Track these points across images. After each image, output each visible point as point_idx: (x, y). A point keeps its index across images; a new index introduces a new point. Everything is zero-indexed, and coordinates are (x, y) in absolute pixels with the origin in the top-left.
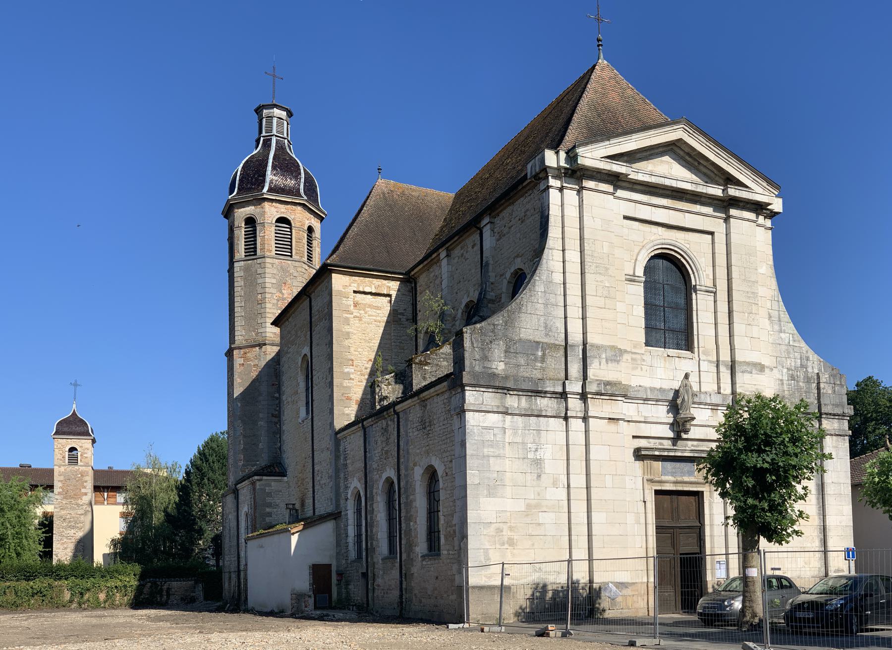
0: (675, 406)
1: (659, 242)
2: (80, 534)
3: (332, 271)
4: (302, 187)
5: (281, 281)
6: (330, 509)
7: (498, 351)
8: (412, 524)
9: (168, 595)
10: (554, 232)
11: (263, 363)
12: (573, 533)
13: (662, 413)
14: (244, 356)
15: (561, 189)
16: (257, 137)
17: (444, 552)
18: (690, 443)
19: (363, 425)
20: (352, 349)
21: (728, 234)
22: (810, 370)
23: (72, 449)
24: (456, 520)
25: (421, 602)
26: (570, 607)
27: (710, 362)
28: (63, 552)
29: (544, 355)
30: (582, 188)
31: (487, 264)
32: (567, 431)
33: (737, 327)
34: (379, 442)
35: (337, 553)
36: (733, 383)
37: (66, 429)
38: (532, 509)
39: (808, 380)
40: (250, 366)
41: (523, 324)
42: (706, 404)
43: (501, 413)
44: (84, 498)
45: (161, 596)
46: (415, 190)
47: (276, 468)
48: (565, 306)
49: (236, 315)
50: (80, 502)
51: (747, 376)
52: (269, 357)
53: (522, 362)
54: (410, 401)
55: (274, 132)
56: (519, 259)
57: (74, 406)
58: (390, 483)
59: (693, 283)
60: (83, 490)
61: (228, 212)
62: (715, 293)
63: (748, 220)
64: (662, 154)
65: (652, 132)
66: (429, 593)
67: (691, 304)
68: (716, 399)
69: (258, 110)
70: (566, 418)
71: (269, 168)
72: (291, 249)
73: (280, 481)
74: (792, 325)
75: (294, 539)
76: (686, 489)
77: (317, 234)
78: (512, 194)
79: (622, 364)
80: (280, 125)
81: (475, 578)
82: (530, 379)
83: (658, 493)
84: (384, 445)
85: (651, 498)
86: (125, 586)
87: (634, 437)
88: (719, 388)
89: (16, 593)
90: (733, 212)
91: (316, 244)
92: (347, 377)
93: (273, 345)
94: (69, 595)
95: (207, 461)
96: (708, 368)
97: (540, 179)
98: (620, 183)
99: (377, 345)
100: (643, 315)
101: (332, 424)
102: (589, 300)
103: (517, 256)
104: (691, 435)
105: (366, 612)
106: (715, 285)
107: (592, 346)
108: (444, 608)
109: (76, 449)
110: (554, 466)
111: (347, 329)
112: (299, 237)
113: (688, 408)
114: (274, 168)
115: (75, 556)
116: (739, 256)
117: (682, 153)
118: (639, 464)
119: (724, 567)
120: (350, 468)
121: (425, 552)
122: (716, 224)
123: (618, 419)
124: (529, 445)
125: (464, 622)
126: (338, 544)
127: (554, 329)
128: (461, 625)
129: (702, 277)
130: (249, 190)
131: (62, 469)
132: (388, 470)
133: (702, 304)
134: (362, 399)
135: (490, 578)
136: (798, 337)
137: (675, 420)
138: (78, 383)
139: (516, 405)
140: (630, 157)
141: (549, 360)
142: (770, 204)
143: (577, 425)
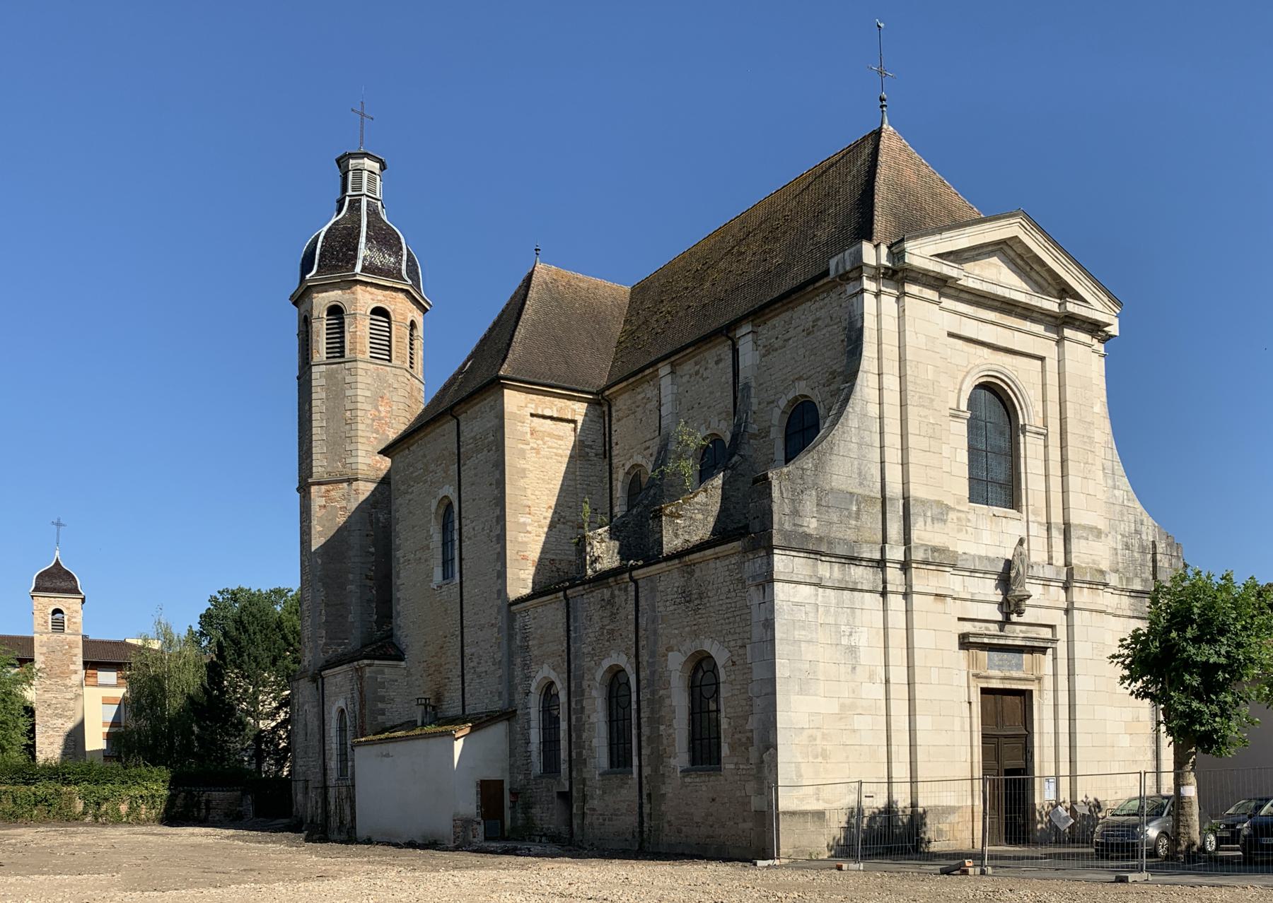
0: (1007, 577)
1: (984, 367)
2: (70, 725)
3: (504, 386)
4: (404, 267)
5: (383, 397)
6: (498, 705)
7: (809, 504)
8: (662, 728)
9: (208, 809)
10: (869, 350)
11: (353, 506)
12: (893, 742)
13: (989, 589)
14: (326, 495)
15: (878, 295)
16: (339, 196)
17: (728, 766)
18: (1018, 628)
19: (565, 596)
20: (529, 492)
21: (1061, 361)
22: (1144, 537)
23: (57, 611)
24: (752, 723)
25: (680, 831)
26: (890, 837)
27: (1040, 524)
28: (49, 748)
29: (859, 510)
30: (905, 294)
31: (747, 387)
32: (885, 610)
33: (1073, 481)
34: (596, 618)
35: (511, 766)
36: (1067, 552)
37: (48, 584)
38: (847, 711)
39: (1143, 551)
40: (334, 508)
41: (835, 470)
42: (1038, 578)
43: (814, 585)
44: (73, 677)
45: (199, 810)
46: (585, 281)
47: (384, 645)
48: (882, 447)
49: (314, 438)
50: (68, 682)
51: (1083, 542)
52: (362, 498)
53: (835, 519)
54: (664, 564)
55: (365, 191)
56: (803, 383)
57: (57, 553)
58: (616, 674)
59: (1021, 422)
60: (72, 667)
61: (301, 298)
62: (1046, 436)
63: (1084, 344)
64: (990, 254)
65: (987, 226)
66: (696, 819)
67: (1018, 449)
68: (1049, 572)
69: (342, 162)
70: (884, 594)
71: (363, 239)
72: (390, 351)
73: (396, 666)
74: (1126, 479)
75: (458, 746)
76: (1008, 686)
77: (420, 332)
78: (794, 297)
79: (949, 524)
80: (371, 181)
81: (787, 800)
82: (845, 542)
83: (985, 691)
84: (606, 621)
85: (976, 697)
86: (153, 796)
87: (960, 619)
88: (1050, 558)
89: (14, 801)
90: (1067, 332)
91: (418, 344)
92: (523, 528)
93: (367, 480)
94: (82, 805)
95: (246, 631)
96: (1038, 531)
97: (848, 279)
98: (946, 290)
99: (558, 487)
100: (966, 461)
101: (502, 590)
102: (912, 441)
103: (800, 379)
104: (1026, 618)
105: (573, 842)
106: (1046, 426)
107: (916, 500)
108: (746, 836)
109: (61, 612)
110: (871, 656)
111: (522, 464)
112: (399, 333)
113: (1023, 585)
114: (368, 239)
115: (64, 754)
116: (1069, 386)
117: (1012, 254)
118: (963, 653)
119: (1053, 786)
120: (535, 652)
121: (687, 765)
122: (1046, 347)
123: (945, 596)
124: (843, 628)
125: (773, 858)
126: (512, 753)
127: (869, 477)
128: (770, 862)
129: (1030, 414)
130: (335, 268)
131: (45, 637)
132: (614, 656)
133: (1031, 448)
134: (540, 559)
135: (802, 800)
136: (1133, 495)
137: (1005, 599)
138: (62, 521)
139: (828, 575)
140: (956, 256)
141: (864, 517)
142: (1109, 325)
143: (896, 602)
